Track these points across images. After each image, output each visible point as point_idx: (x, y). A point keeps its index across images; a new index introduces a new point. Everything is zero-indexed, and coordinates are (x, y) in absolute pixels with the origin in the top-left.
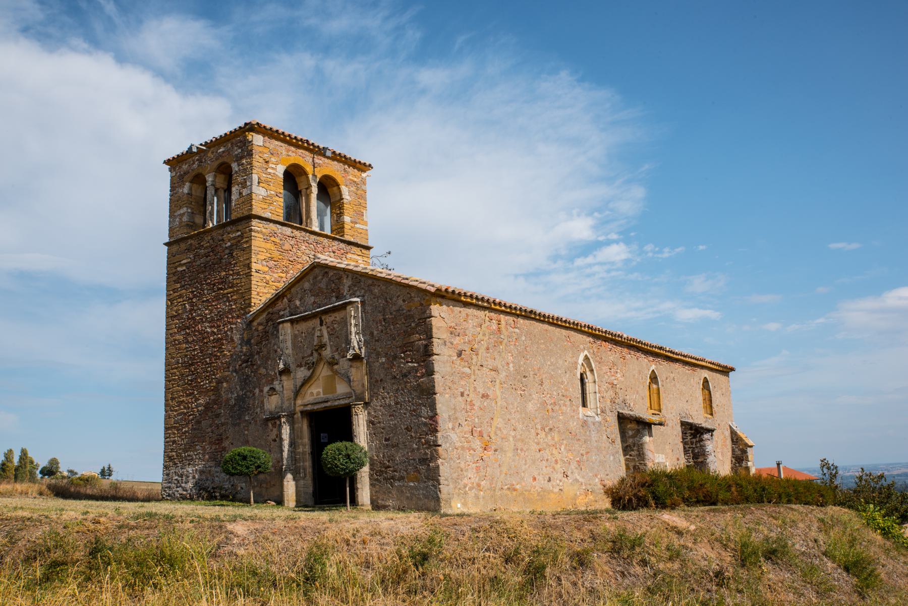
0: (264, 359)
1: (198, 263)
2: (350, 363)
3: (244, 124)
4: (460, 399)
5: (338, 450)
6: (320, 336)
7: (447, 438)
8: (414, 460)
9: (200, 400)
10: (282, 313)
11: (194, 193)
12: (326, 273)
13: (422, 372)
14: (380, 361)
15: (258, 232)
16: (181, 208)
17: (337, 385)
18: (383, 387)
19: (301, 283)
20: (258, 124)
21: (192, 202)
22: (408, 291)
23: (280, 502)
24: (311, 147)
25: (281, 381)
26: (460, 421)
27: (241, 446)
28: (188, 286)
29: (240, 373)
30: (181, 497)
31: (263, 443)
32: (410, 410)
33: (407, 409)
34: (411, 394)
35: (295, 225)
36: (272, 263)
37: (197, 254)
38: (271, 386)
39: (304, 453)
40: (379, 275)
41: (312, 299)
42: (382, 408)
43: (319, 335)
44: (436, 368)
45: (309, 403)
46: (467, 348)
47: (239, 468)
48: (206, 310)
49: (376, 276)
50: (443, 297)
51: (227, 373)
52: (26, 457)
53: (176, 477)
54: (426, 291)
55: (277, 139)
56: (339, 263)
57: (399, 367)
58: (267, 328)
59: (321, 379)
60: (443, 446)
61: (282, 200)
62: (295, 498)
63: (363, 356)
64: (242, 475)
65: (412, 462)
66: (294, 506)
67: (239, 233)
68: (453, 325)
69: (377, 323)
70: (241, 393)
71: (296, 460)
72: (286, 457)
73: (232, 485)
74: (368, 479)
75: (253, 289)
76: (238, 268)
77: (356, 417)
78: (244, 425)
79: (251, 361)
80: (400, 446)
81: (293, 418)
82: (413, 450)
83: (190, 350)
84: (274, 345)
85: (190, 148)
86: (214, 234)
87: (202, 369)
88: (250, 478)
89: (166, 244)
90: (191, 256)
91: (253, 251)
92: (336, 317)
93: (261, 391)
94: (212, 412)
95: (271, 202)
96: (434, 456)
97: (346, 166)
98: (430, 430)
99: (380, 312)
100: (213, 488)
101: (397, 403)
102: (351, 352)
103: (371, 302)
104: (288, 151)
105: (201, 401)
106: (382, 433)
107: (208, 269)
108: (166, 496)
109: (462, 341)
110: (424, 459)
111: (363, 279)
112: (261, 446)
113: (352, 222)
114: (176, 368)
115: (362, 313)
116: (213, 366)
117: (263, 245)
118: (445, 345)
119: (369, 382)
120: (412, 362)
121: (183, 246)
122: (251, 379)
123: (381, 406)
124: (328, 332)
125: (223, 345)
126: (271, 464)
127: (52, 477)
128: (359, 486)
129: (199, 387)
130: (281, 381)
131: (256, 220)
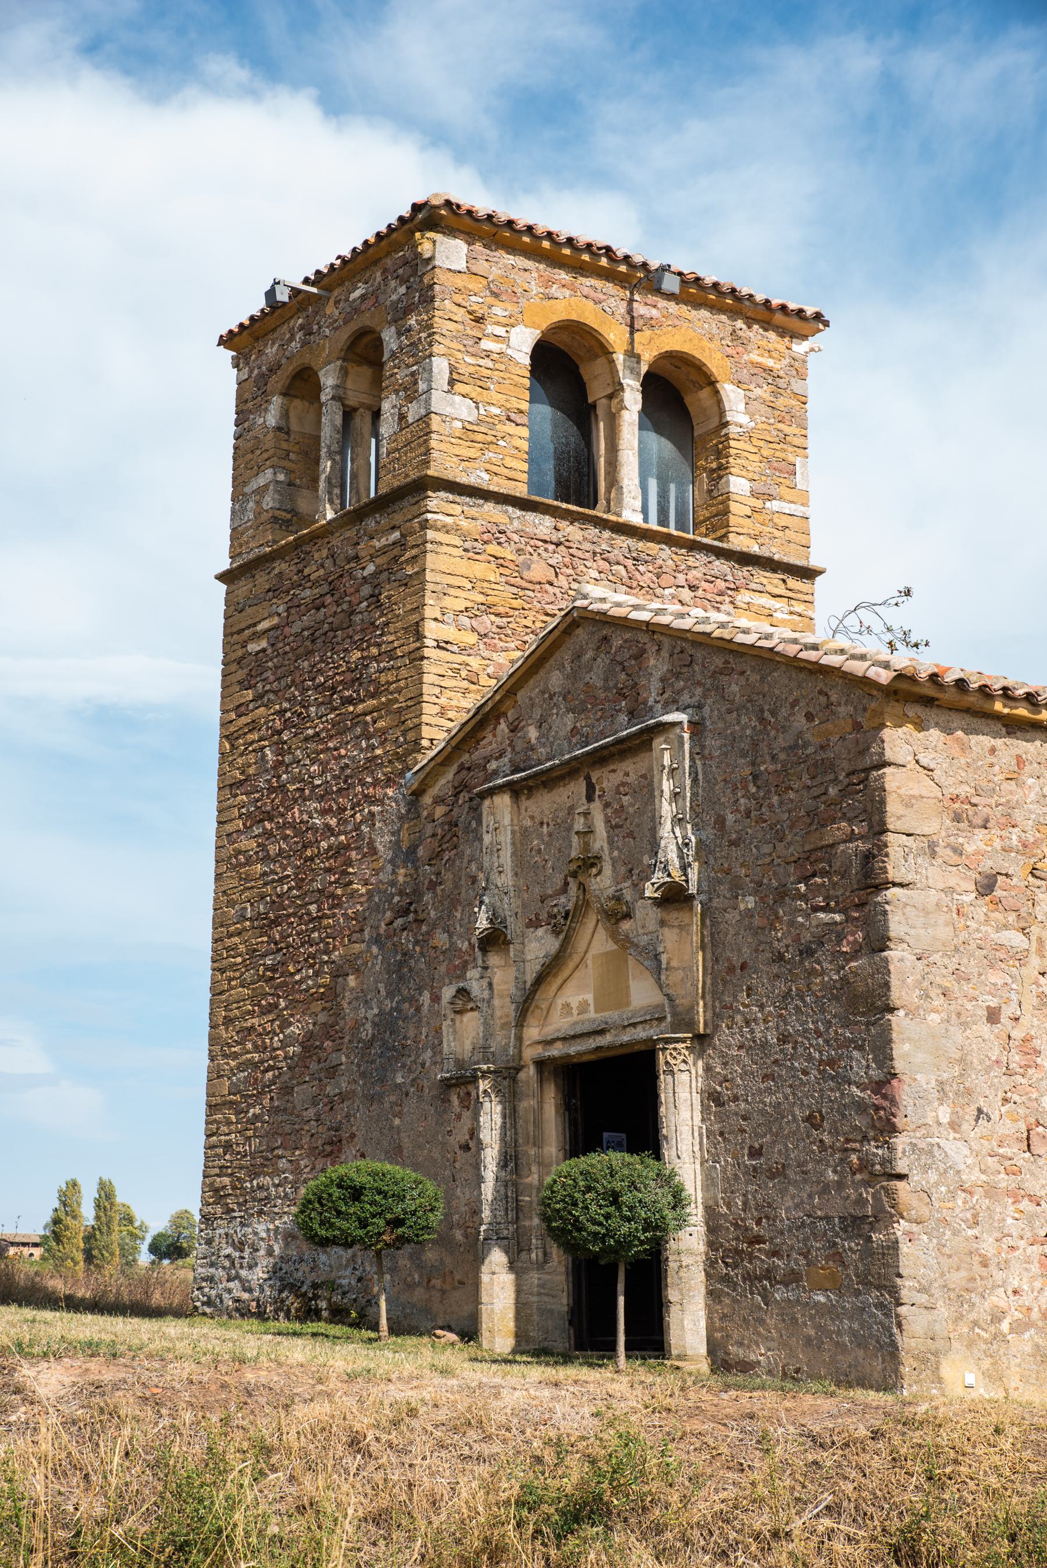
1: (296, 628)
3: (409, 208)
4: (985, 1029)
7: (930, 1153)
8: (828, 1218)
9: (290, 1024)
10: (493, 765)
11: (294, 426)
12: (605, 639)
13: (856, 941)
14: (742, 907)
15: (446, 529)
16: (260, 469)
17: (631, 982)
18: (749, 989)
19: (542, 673)
20: (448, 203)
21: (288, 452)
22: (820, 685)
23: (469, 1333)
24: (623, 268)
25: (486, 968)
26: (982, 1102)
28: (272, 696)
30: (237, 1310)
32: (821, 1061)
33: (810, 1058)
34: (823, 1011)
36: (487, 622)
37: (296, 602)
40: (740, 638)
42: (742, 1053)
44: (896, 926)
46: (1017, 867)
49: (730, 641)
50: (928, 702)
51: (357, 947)
52: (112, 1204)
53: (229, 1250)
54: (865, 682)
55: (513, 249)
56: (636, 607)
57: (792, 923)
59: (589, 962)
60: (915, 1177)
61: (525, 432)
62: (511, 1325)
63: (693, 890)
65: (821, 1225)
66: (508, 1350)
67: (397, 535)
68: (964, 790)
70: (388, 1005)
72: (490, 1198)
75: (425, 698)
76: (391, 638)
77: (669, 1078)
79: (416, 912)
80: (791, 1173)
81: (514, 1080)
82: (825, 1189)
83: (273, 881)
84: (470, 862)
85: (270, 294)
86: (336, 541)
87: (298, 934)
89: (222, 577)
90: (281, 609)
91: (429, 587)
92: (627, 774)
93: (436, 999)
94: (319, 1062)
95: (489, 438)
96: (884, 1211)
97: (740, 324)
98: (874, 1127)
99: (743, 754)
100: (315, 1286)
101: (783, 1039)
102: (659, 877)
103: (721, 725)
104: (548, 283)
105: (294, 1029)
107: (319, 643)
108: (203, 1304)
109: (997, 844)
110: (855, 1218)
111: (699, 655)
113: (754, 494)
114: (239, 933)
115: (692, 759)
116: (326, 928)
117: (463, 566)
118: (933, 854)
120: (826, 909)
121: (262, 580)
123: (740, 1047)
124: (607, 821)
125: (351, 865)
127: (180, 1262)
128: (672, 1294)
129: (289, 988)
130: (486, 968)
131: (442, 494)
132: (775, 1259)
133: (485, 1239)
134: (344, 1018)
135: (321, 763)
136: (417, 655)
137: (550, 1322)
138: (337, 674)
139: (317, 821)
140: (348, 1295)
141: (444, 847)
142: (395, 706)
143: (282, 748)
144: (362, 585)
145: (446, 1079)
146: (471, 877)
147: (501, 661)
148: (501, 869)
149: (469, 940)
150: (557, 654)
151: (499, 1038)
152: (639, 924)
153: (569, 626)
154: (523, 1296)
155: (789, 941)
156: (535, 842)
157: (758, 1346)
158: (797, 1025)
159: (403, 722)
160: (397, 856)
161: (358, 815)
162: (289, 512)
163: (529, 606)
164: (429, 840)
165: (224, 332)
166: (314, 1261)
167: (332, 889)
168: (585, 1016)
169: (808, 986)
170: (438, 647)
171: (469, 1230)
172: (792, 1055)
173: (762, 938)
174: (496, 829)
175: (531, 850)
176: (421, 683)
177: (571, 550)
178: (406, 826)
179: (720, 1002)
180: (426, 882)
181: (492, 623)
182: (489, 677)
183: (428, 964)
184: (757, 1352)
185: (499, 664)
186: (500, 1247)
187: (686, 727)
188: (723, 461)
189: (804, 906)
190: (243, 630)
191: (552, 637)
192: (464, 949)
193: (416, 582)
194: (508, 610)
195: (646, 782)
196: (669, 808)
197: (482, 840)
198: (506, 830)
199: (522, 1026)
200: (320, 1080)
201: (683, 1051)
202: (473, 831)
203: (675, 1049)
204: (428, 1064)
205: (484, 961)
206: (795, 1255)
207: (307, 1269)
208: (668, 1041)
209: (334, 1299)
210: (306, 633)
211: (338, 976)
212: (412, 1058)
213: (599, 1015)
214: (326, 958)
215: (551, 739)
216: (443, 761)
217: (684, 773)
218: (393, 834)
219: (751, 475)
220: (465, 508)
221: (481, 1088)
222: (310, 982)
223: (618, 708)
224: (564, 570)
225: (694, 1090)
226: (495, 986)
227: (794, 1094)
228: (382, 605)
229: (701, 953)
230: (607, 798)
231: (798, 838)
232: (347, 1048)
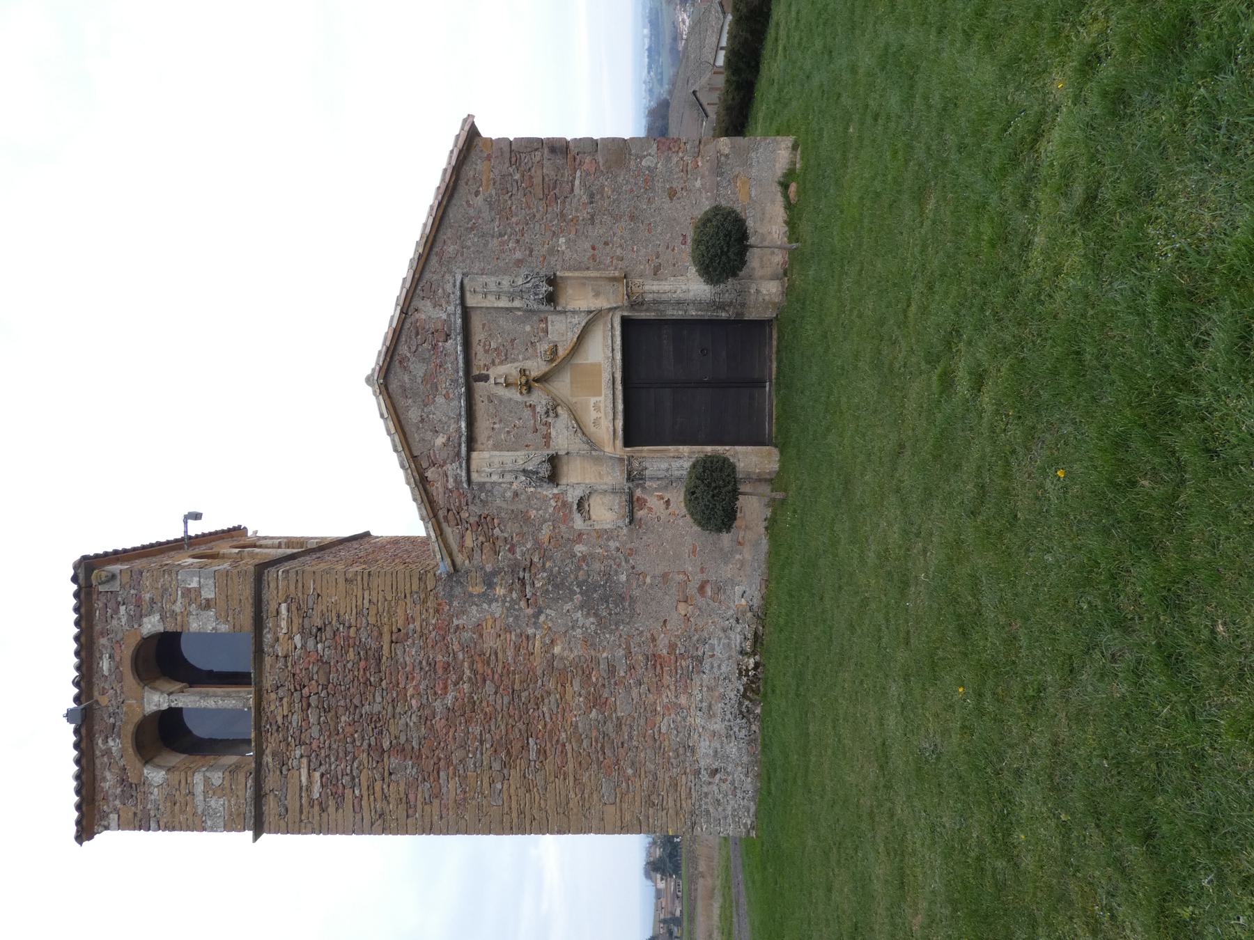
17: (589, 362)
38: (575, 507)
124: (501, 363)
165: (73, 829)
168: (602, 405)
173: (581, 231)
190: (301, 806)
204: (618, 545)
212: (612, 562)
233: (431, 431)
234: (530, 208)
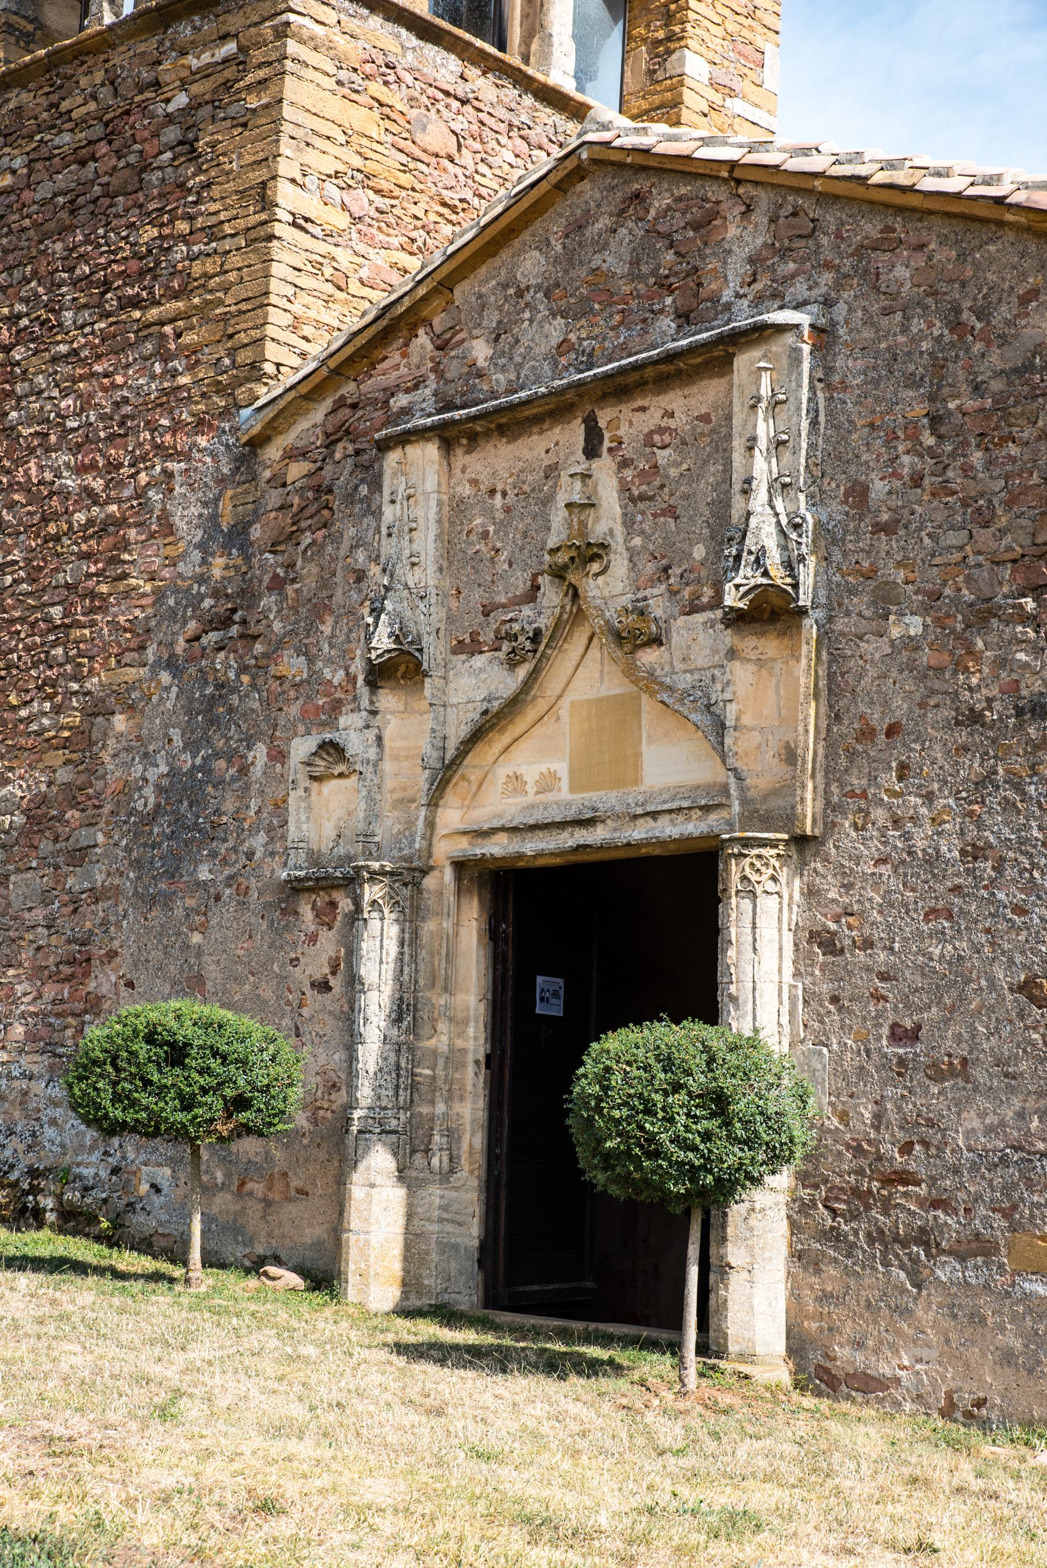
0: (303, 611)
1: (44, 191)
2: (728, 637)
5: (668, 1063)
6: (584, 506)
10: (401, 401)
14: (895, 632)
19: (505, 255)
25: (374, 713)
27: (165, 999)
29: (192, 670)
31: (267, 992)
35: (478, 43)
36: (362, 200)
37: (44, 152)
38: (328, 736)
39: (454, 1058)
41: (555, 330)
43: (576, 498)
45: (496, 823)
47: (145, 1099)
48: (65, 394)
58: (329, 469)
59: (564, 713)
62: (396, 1267)
64: (156, 1133)
66: (389, 1306)
67: (230, 47)
69: (891, 439)
70: (186, 761)
71: (414, 1087)
73: (115, 1171)
74: (783, 1227)
75: (273, 299)
76: (213, 207)
77: (746, 904)
78: (191, 902)
79: (244, 622)
80: (980, 1075)
81: (417, 885)
84: (353, 548)
86: (119, 58)
87: (28, 649)
88: (196, 1152)
90: (17, 163)
91: (287, 128)
93: (279, 756)
94: (56, 840)
99: (912, 382)
100: (33, 1173)
101: (974, 852)
102: (747, 576)
103: (867, 334)
106: (878, 997)
107: (83, 215)
111: (830, 218)
112: (256, 1006)
115: (812, 388)
116: (77, 642)
117: (335, 107)
119: (829, 740)
122: (235, 700)
123: (881, 861)
124: (624, 488)
126: (296, 1094)
128: (734, 1253)
130: (374, 713)
132: (939, 1213)
133: (360, 1132)
134: (103, 777)
135: (80, 396)
136: (261, 232)
137: (453, 1264)
138: (115, 261)
139: (69, 482)
140: (94, 1192)
141: (304, 524)
142: (218, 311)
143: (12, 372)
144: (164, 126)
145: (298, 879)
146: (355, 571)
147: (379, 262)
148: (414, 560)
149: (347, 669)
150: (538, 224)
151: (388, 822)
152: (677, 654)
153: (568, 176)
154: (416, 1222)
155: (995, 691)
156: (478, 521)
157: (897, 1353)
158: (1006, 831)
159: (231, 336)
160: (211, 538)
161: (143, 475)
162: (31, 22)
163: (422, 187)
164: (273, 515)
166: (34, 1135)
167: (90, 584)
168: (550, 797)
169: (1032, 767)
170: (294, 224)
171: (321, 1113)
172: (992, 881)
173: (937, 685)
174: (409, 497)
175: (469, 532)
176: (268, 276)
177: (480, 114)
178: (230, 493)
179: (842, 786)
180: (267, 579)
181: (371, 202)
182: (362, 283)
183: (266, 703)
184: (895, 1362)
185: (376, 266)
186: (385, 1144)
187: (806, 333)
188: (677, 29)
189: (1032, 635)
191: (535, 193)
192: (336, 682)
193: (263, 121)
194: (392, 187)
195: (708, 427)
196: (765, 466)
197: (381, 513)
198: (427, 499)
199: (437, 805)
200: (57, 867)
201: (773, 861)
202: (361, 501)
203: (759, 857)
204: (258, 855)
205: (372, 702)
206: (983, 1211)
207: (21, 1147)
208: (747, 843)
209: (68, 1196)
210: (61, 200)
211: (95, 715)
212: (230, 844)
213: (577, 796)
214: (75, 686)
215: (518, 359)
216: (310, 392)
217: (799, 409)
218: (205, 504)
219: (711, 55)
220: (342, 17)
221: (367, 897)
222: (46, 721)
223: (656, 307)
224: (470, 141)
225: (785, 926)
226: (386, 742)
227: (992, 944)
228: (200, 156)
229: (813, 704)
230: (627, 451)
231: (1023, 522)
232: (107, 823)
233: (500, 322)
234: (1008, 504)
